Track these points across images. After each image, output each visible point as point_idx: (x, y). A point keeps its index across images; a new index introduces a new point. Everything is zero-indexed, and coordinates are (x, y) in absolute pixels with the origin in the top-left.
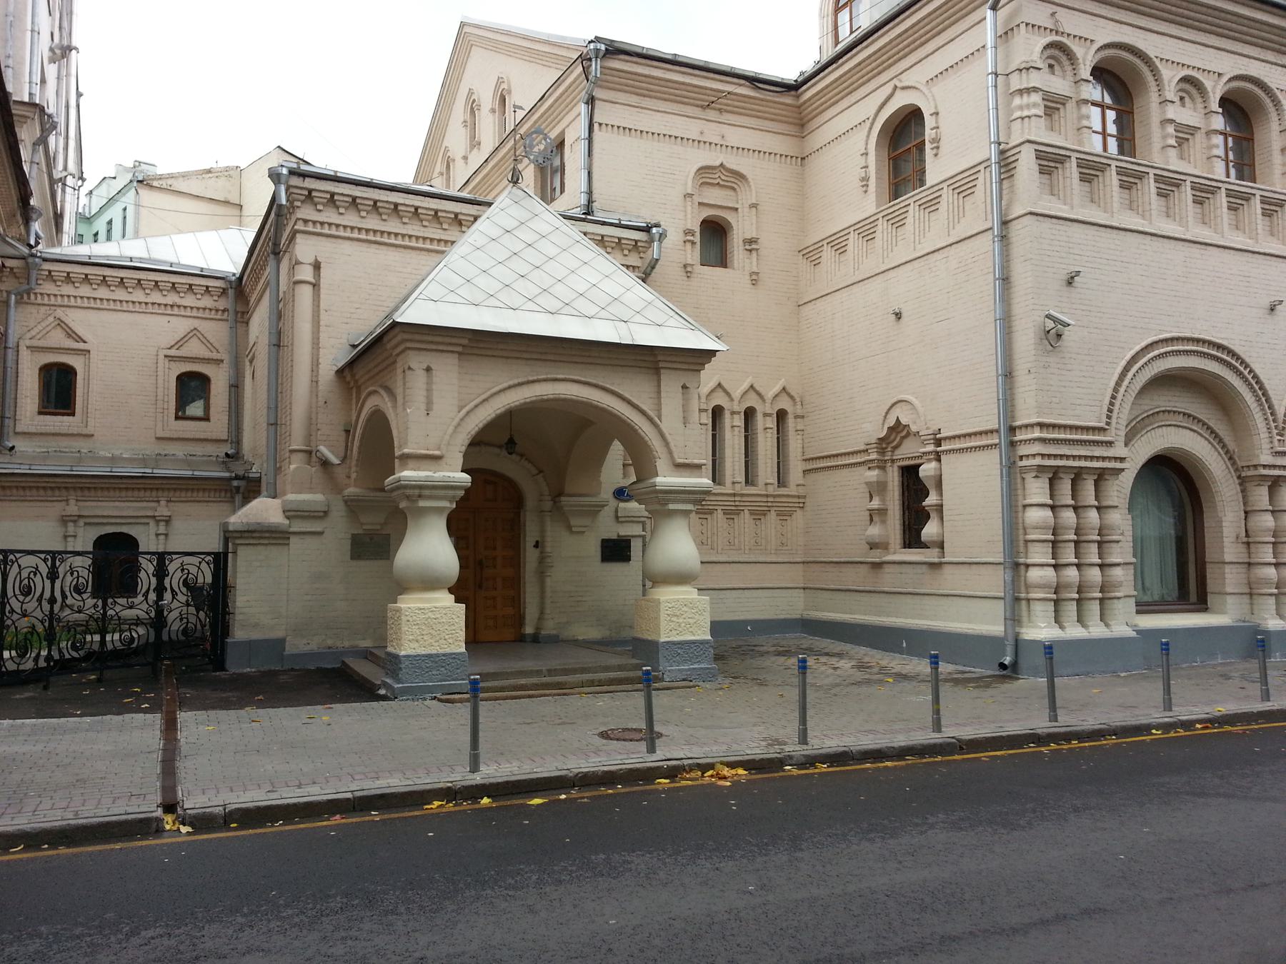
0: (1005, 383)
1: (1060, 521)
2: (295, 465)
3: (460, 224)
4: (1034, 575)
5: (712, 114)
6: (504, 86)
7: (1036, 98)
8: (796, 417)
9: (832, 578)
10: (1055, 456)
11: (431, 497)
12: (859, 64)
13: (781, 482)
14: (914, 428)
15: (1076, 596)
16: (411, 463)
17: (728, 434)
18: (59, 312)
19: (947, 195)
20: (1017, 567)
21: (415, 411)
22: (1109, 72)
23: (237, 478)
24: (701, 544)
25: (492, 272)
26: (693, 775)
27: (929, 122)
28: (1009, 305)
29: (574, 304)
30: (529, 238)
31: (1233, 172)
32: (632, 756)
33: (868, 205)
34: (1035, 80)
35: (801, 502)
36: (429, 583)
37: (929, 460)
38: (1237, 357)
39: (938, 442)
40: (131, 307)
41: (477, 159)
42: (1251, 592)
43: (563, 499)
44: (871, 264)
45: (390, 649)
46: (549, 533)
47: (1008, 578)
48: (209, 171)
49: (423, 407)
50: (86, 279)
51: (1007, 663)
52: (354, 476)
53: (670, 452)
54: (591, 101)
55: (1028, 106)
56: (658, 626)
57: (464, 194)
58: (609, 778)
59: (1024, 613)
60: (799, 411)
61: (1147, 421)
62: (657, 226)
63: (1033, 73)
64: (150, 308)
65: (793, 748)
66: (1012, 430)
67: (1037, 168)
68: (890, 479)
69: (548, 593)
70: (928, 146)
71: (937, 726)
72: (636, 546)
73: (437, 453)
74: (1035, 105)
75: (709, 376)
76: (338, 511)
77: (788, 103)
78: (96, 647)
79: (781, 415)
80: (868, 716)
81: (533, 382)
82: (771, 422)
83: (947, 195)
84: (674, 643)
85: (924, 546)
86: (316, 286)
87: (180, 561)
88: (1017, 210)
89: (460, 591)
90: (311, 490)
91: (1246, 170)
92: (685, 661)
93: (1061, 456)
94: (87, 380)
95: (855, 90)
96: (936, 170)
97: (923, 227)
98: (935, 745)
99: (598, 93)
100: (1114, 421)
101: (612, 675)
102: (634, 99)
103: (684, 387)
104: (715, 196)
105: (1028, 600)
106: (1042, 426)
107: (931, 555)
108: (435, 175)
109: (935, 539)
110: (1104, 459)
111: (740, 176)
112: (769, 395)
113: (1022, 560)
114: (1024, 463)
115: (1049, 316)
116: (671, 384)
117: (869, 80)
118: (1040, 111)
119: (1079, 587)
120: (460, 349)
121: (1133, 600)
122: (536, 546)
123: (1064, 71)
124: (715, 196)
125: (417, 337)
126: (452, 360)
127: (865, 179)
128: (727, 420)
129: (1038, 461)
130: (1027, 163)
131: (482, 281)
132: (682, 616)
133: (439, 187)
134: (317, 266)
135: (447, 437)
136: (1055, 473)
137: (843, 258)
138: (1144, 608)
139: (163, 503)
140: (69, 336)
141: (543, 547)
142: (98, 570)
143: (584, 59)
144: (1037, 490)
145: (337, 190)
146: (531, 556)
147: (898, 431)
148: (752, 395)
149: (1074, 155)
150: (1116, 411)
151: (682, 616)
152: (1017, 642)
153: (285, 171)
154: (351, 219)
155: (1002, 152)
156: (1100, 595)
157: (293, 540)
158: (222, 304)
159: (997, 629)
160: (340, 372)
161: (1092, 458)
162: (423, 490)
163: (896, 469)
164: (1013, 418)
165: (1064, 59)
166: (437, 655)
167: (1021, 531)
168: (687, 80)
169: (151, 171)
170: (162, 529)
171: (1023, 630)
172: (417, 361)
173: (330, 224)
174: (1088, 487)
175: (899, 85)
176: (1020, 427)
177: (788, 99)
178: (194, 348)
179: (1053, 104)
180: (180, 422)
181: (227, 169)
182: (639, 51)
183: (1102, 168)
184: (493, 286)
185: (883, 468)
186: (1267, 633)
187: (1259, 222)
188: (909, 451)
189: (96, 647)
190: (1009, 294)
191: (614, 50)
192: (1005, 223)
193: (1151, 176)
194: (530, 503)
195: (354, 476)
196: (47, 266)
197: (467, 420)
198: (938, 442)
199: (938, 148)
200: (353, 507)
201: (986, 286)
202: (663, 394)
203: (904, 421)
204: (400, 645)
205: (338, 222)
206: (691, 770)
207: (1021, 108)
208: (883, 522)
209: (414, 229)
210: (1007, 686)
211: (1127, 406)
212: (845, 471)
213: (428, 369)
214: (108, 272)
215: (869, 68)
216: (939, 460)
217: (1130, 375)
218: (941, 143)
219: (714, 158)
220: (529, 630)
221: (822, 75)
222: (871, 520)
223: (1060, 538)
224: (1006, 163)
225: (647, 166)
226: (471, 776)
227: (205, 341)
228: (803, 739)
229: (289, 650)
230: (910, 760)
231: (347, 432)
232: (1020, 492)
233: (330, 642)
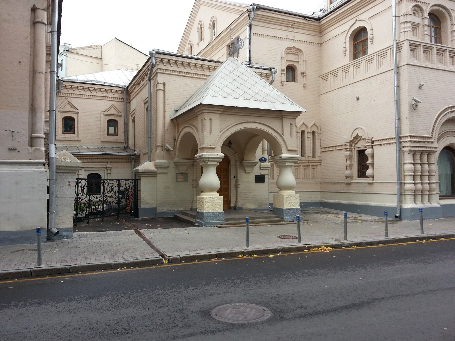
0: (398, 122)
1: (416, 168)
3: (209, 69)
4: (407, 186)
5: (290, 29)
6: (215, 19)
7: (409, 25)
8: (318, 133)
9: (331, 188)
10: (415, 147)
11: (212, 161)
12: (343, 12)
13: (313, 156)
14: (363, 137)
15: (421, 193)
16: (205, 150)
17: (306, 141)
18: (69, 99)
19: (376, 57)
20: (401, 184)
21: (206, 133)
22: (436, 16)
23: (132, 155)
24: (296, 177)
25: (228, 86)
26: (315, 249)
27: (369, 32)
28: (399, 95)
29: (255, 97)
30: (238, 74)
31: (433, 40)
32: (295, 244)
33: (346, 60)
34: (409, 18)
35: (320, 163)
36: (211, 189)
39: (372, 142)
40: (92, 97)
41: (203, 45)
43: (244, 162)
44: (346, 82)
45: (198, 210)
46: (238, 173)
47: (398, 187)
48: (91, 47)
49: (209, 131)
50: (77, 87)
51: (398, 216)
52: (177, 154)
53: (286, 146)
54: (250, 25)
55: (407, 28)
56: (283, 203)
57: (199, 57)
58: (283, 250)
59: (403, 199)
60: (319, 132)
61: (444, 135)
62: (274, 68)
63: (409, 16)
64: (98, 98)
65: (343, 241)
66: (400, 138)
67: (409, 49)
68: (354, 154)
69: (239, 193)
70: (369, 41)
71: (387, 235)
72: (266, 178)
73: (214, 147)
74: (409, 27)
75: (299, 121)
76: (172, 165)
77: (317, 24)
78: (101, 210)
79: (313, 133)
80: (365, 231)
81: (243, 123)
82: (310, 135)
83: (376, 57)
84: (288, 209)
85: (367, 177)
86: (164, 91)
87: (124, 182)
88: (402, 63)
89: (220, 192)
90: (163, 159)
91: (438, 40)
92: (292, 215)
93: (417, 147)
94: (79, 122)
95: (341, 20)
96: (371, 49)
97: (365, 68)
98: (388, 241)
99: (253, 23)
100: (434, 135)
101: (269, 219)
102: (265, 25)
103: (291, 124)
104: (292, 57)
105: (405, 195)
106: (411, 136)
107: (370, 180)
108: (186, 49)
109: (371, 175)
110: (430, 147)
112: (309, 126)
113: (403, 182)
114: (404, 149)
115: (413, 100)
116: (286, 122)
117: (346, 17)
118: (410, 29)
119: (422, 190)
120: (220, 112)
121: (438, 195)
122: (234, 177)
123: (419, 15)
124: (292, 57)
125: (207, 108)
126: (218, 115)
127: (345, 51)
128: (306, 134)
129: (409, 148)
130: (406, 47)
131: (226, 89)
132: (291, 200)
133: (186, 53)
134: (164, 84)
135: (217, 141)
136: (415, 152)
137: (336, 78)
138: (442, 197)
139: (109, 163)
140: (72, 107)
141: (237, 178)
142: (89, 185)
143: (249, 11)
144: (408, 158)
145: (171, 58)
146: (233, 181)
148: (304, 126)
149: (422, 44)
150: (434, 132)
151: (291, 200)
152: (401, 209)
153: (155, 52)
154: (174, 68)
155: (397, 43)
156: (428, 193)
158: (121, 96)
159: (393, 204)
160: (172, 120)
161: (427, 147)
162: (210, 159)
163: (356, 151)
164: (400, 134)
165: (419, 10)
166: (215, 213)
167: (403, 172)
168: (283, 17)
169: (70, 47)
170: (109, 172)
171: (403, 205)
172: (207, 116)
173: (168, 70)
175: (358, 19)
176: (403, 137)
177: (316, 23)
178: (113, 111)
179: (415, 27)
180: (108, 136)
181: (97, 46)
182: (267, 8)
183: (431, 48)
184: (229, 91)
185: (351, 151)
187: (435, 57)
188: (361, 145)
189: (101, 210)
190: (399, 92)
191: (259, 8)
192: (398, 68)
193: (448, 50)
194: (232, 163)
195: (177, 154)
196: (64, 83)
197: (223, 136)
198: (372, 142)
199: (372, 41)
200: (177, 164)
201: (392, 89)
202: (284, 127)
203: (359, 135)
204: (203, 210)
205: (191, 72)
206: (314, 248)
207: (404, 28)
208: (351, 169)
209: (194, 71)
210: (399, 223)
211: (438, 129)
212: (337, 152)
213: (210, 119)
214: (84, 85)
215: (347, 13)
216: (373, 148)
217: (439, 119)
218: (374, 40)
219: (291, 44)
220: (232, 205)
221: (329, 15)
222: (347, 168)
223: (416, 174)
224: (399, 47)
225: (270, 48)
226: (247, 248)
227: (116, 109)
228: (346, 238)
229: (158, 211)
230: (381, 245)
231: (175, 140)
232: (402, 159)
233: (170, 209)
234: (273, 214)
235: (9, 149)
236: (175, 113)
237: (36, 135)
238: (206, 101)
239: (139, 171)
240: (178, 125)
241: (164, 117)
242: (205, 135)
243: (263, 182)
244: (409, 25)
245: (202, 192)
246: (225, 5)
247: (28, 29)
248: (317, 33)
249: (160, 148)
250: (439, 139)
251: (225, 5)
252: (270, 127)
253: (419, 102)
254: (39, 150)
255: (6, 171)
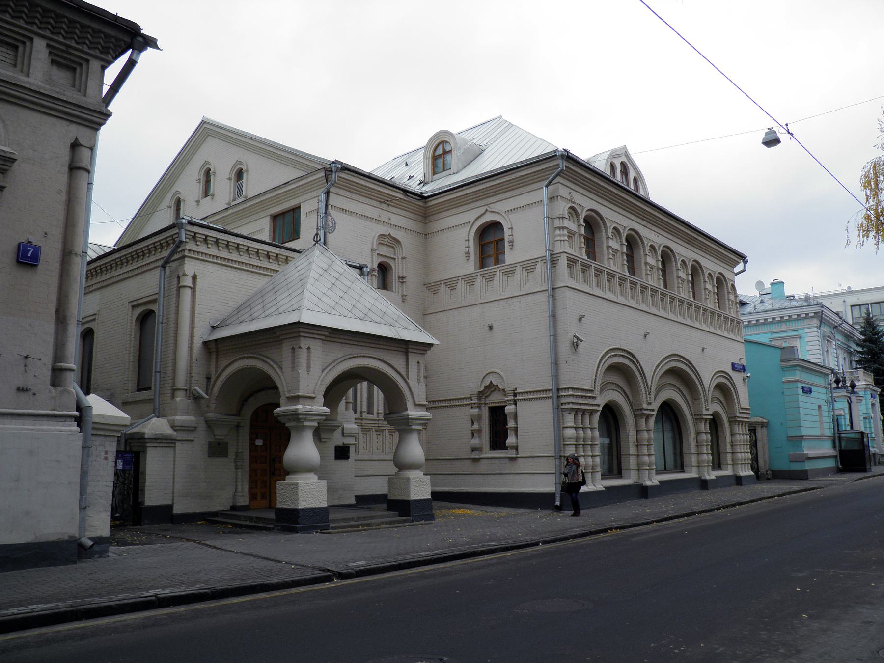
2: (180, 398)
3: (269, 258)
5: (384, 206)
7: (566, 232)
14: (501, 387)
27: (507, 233)
33: (470, 267)
37: (510, 404)
38: (636, 358)
39: (515, 395)
42: (734, 464)
54: (327, 193)
70: (506, 244)
72: (352, 450)
76: (202, 427)
85: (505, 448)
86: (193, 289)
96: (510, 257)
97: (500, 285)
102: (348, 194)
103: (418, 363)
104: (384, 250)
107: (511, 453)
110: (593, 405)
111: (397, 241)
114: (564, 406)
115: (575, 336)
120: (323, 338)
125: (306, 330)
127: (468, 253)
129: (571, 406)
130: (563, 262)
134: (194, 278)
147: (491, 388)
154: (213, 251)
155: (551, 255)
157: (178, 444)
160: (205, 343)
174: (587, 418)
177: (420, 203)
185: (479, 407)
186: (647, 487)
188: (495, 399)
191: (345, 168)
192: (553, 289)
198: (515, 395)
200: (210, 425)
203: (494, 383)
207: (560, 236)
209: (244, 259)
216: (515, 404)
222: (473, 435)
234: (388, 510)
235: (18, 389)
236: (212, 332)
237: (64, 365)
238: (305, 319)
239: (146, 436)
240: (217, 352)
241: (192, 336)
242: (301, 375)
243: (347, 457)
244: (566, 232)
245: (288, 474)
246: (273, 150)
247: (64, 178)
248: (420, 218)
249: (182, 393)
250: (601, 391)
251: (273, 150)
252: (386, 364)
253: (581, 341)
254: (69, 392)
255: (12, 429)
